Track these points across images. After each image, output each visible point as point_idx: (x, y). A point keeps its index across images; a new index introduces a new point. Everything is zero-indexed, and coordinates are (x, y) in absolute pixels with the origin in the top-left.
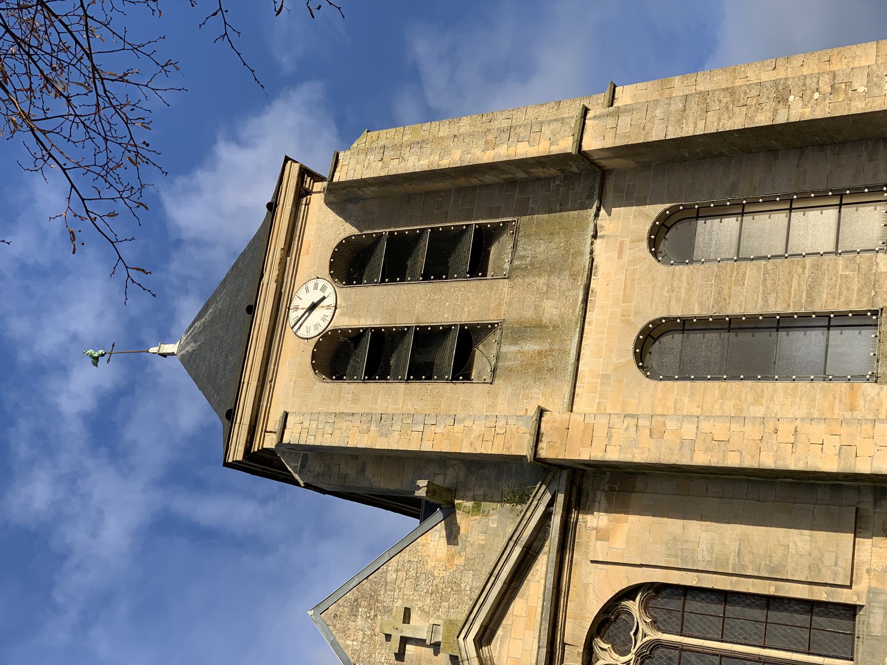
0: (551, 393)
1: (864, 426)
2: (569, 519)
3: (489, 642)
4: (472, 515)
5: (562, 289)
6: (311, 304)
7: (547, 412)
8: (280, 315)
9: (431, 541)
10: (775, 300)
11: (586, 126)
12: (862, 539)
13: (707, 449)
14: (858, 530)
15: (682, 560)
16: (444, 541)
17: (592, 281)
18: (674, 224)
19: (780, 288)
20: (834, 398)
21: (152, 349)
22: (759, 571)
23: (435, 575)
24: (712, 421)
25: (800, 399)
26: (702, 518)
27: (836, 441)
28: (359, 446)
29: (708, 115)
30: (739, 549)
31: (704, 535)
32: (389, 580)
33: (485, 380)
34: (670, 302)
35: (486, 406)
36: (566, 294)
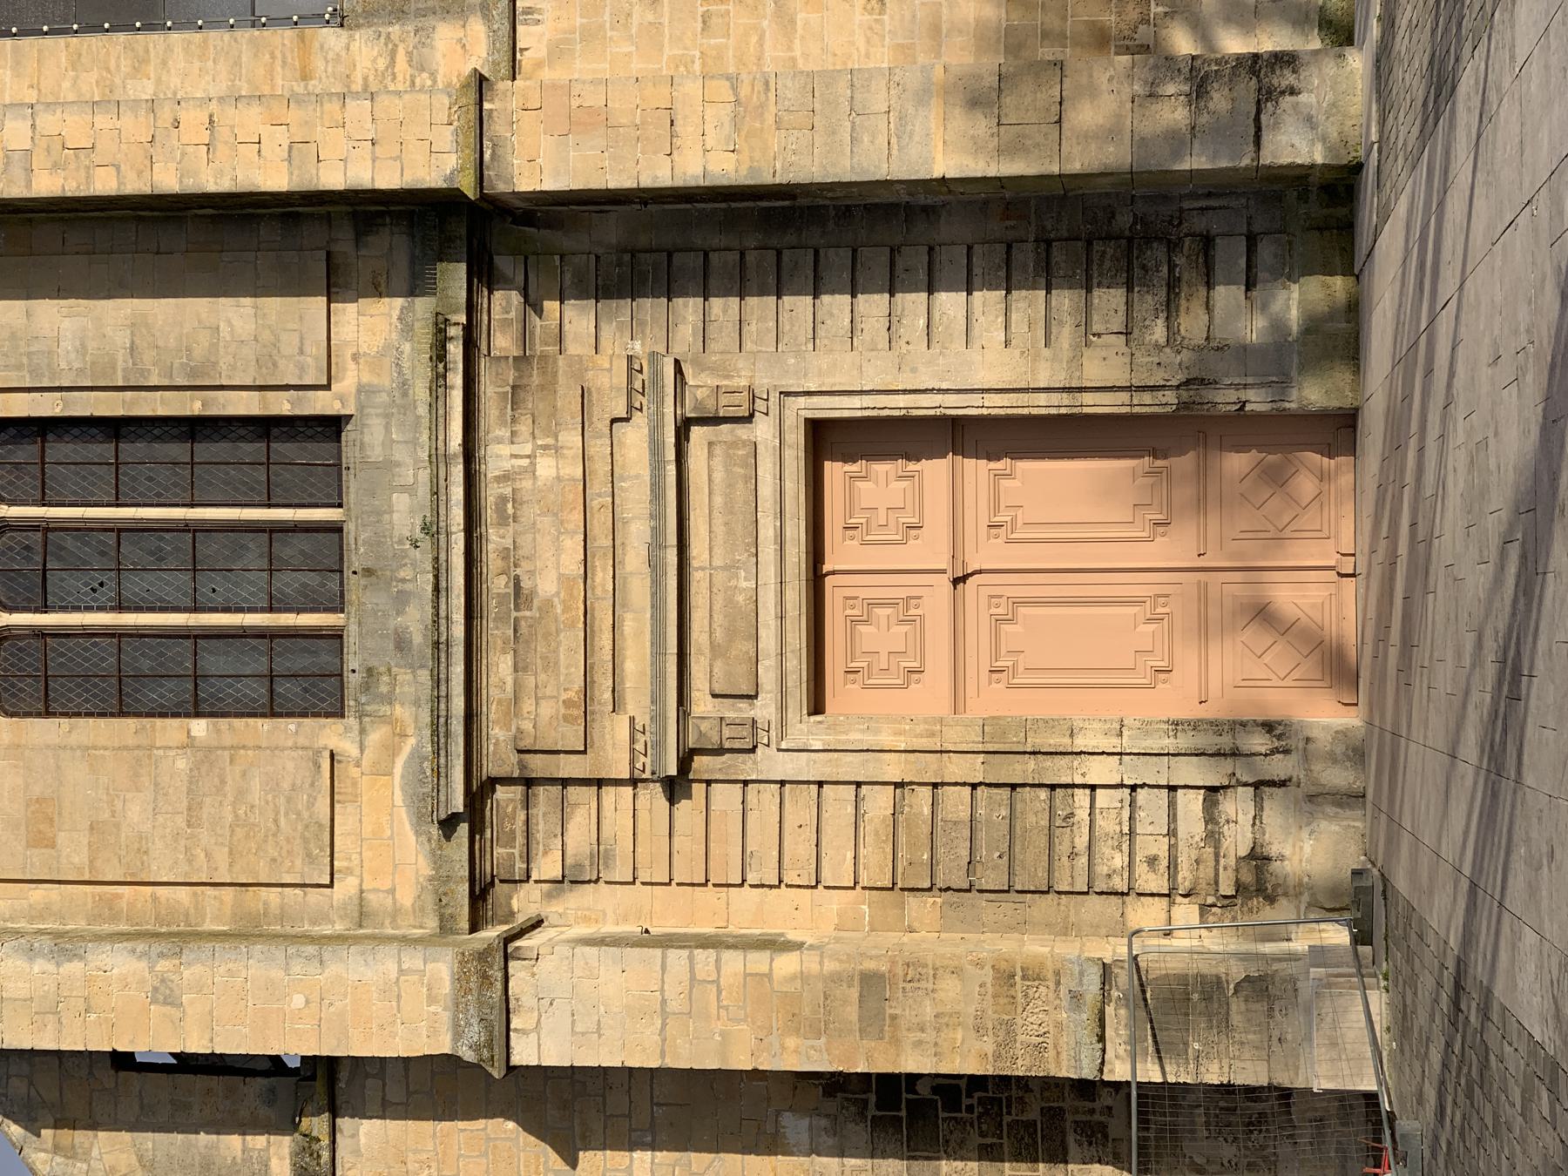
1: (327, 106)
13: (56, 166)
14: (333, 290)
20: (273, 57)
26: (60, 293)
30: (133, 342)
31: (66, 323)
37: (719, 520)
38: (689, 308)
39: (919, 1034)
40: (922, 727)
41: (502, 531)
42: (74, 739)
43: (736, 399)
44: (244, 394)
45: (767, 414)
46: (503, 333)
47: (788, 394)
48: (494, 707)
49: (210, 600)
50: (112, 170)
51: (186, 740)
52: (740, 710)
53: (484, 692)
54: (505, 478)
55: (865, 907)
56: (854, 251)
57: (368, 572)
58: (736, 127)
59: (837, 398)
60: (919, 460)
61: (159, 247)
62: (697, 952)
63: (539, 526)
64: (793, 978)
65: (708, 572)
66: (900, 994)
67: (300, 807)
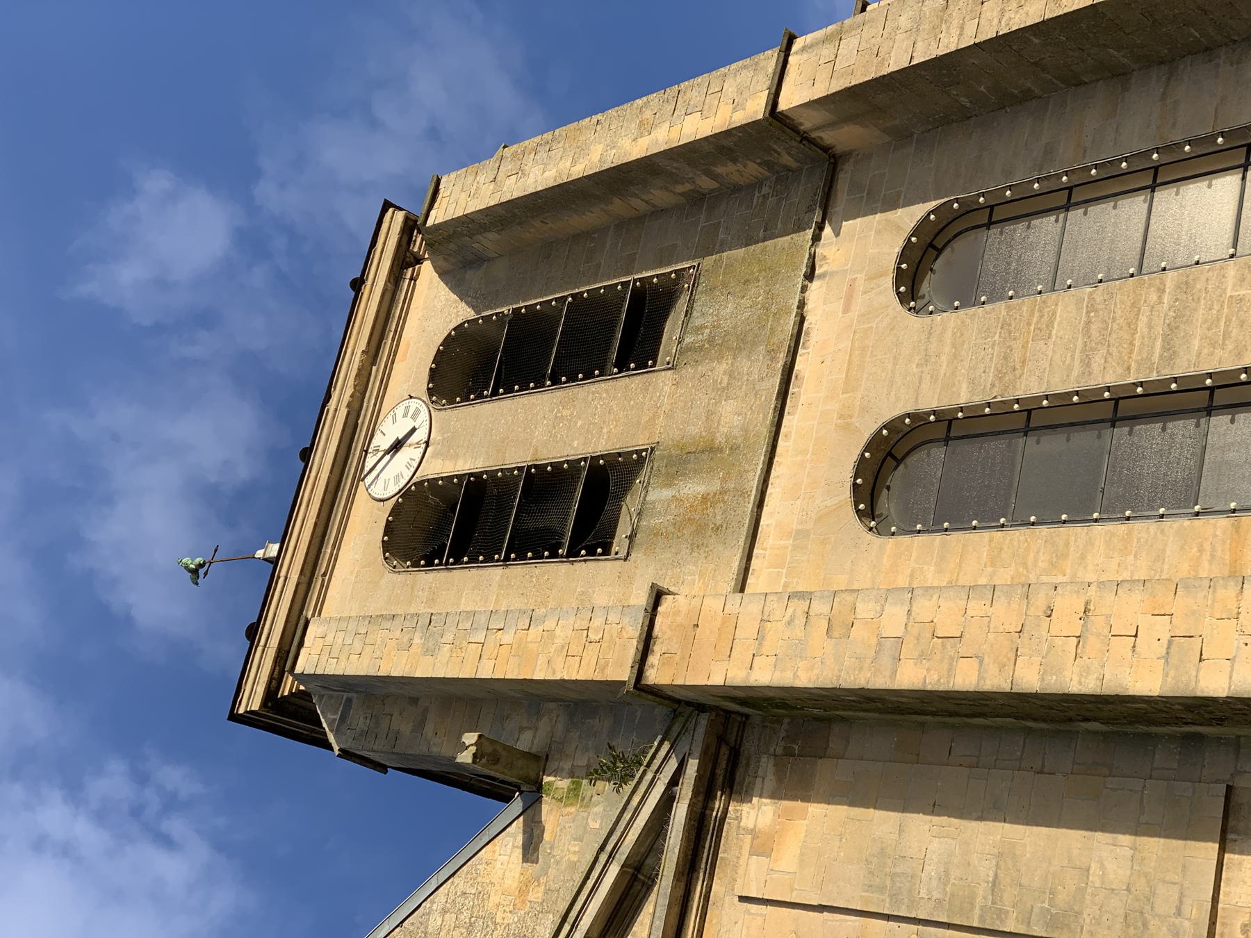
0: (713, 572)
1: (1221, 593)
2: (708, 812)
4: (565, 806)
5: (751, 379)
6: (395, 441)
7: (668, 596)
8: (352, 462)
9: (500, 855)
10: (1103, 361)
11: (788, 66)
12: (1236, 856)
14: (1231, 836)
15: (891, 896)
16: (518, 853)
18: (949, 241)
19: (1114, 336)
20: (1201, 550)
21: (258, 552)
22: (1029, 923)
23: (497, 921)
24: (935, 597)
25: (1135, 556)
26: (934, 809)
27: (1162, 627)
28: (393, 674)
29: (985, 9)
30: (996, 875)
31: (935, 845)
33: (617, 553)
34: (920, 383)
35: (613, 600)
36: (757, 387)
50: (975, 662)
61: (1043, 765)
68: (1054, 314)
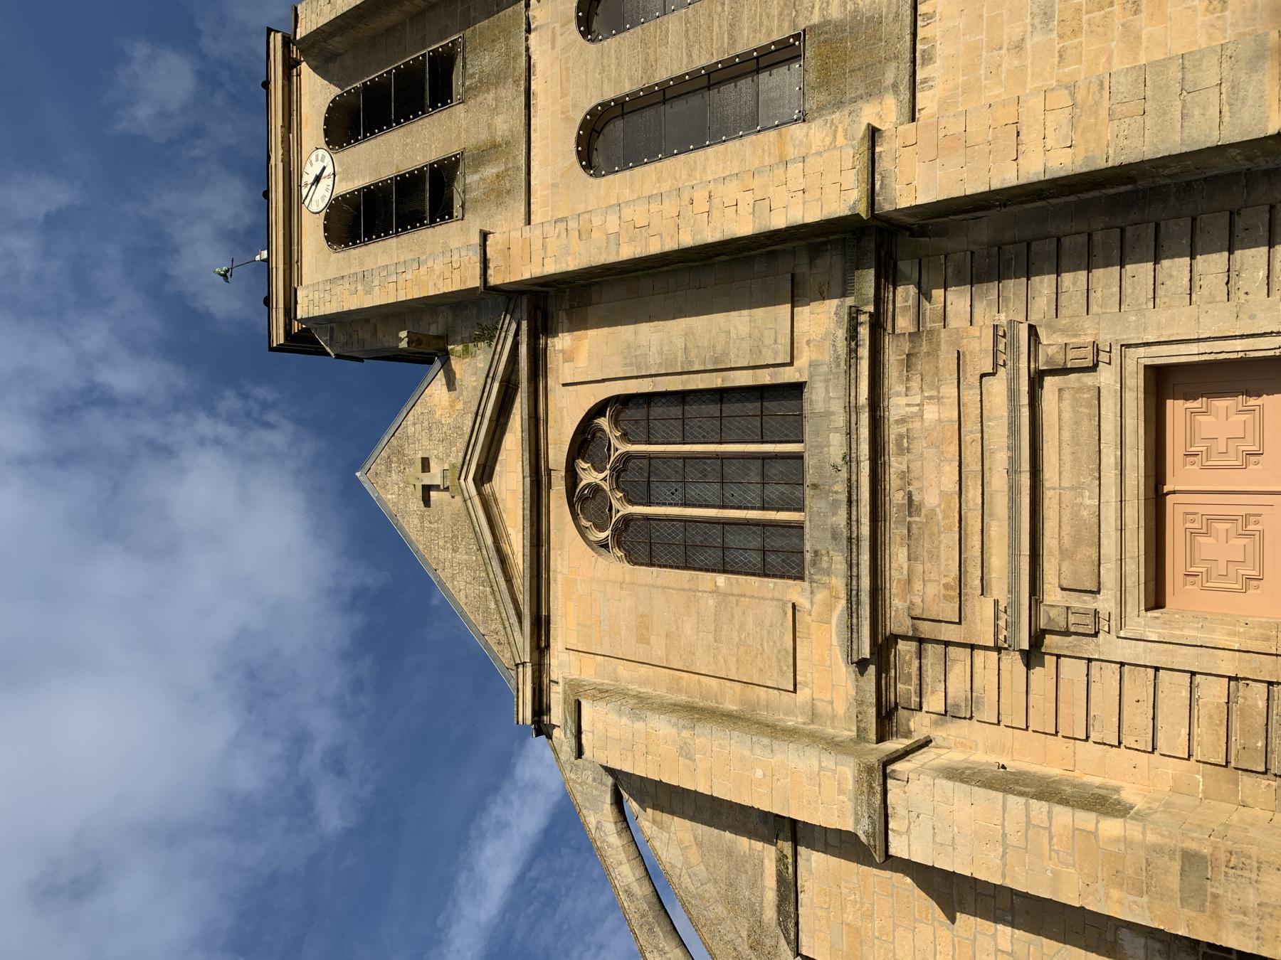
1: (776, 172)
3: (490, 479)
13: (631, 240)
16: (445, 388)
17: (532, 82)
20: (763, 151)
24: (632, 207)
26: (651, 319)
27: (749, 198)
28: (352, 308)
31: (654, 337)
32: (409, 434)
37: (1067, 450)
38: (1044, 284)
39: (1241, 916)
40: (1257, 631)
41: (900, 459)
42: (659, 582)
43: (1082, 353)
44: (745, 372)
45: (1110, 364)
46: (903, 316)
47: (1129, 346)
48: (895, 584)
49: (731, 501)
50: (658, 237)
51: (714, 588)
52: (1085, 602)
53: (888, 573)
54: (902, 421)
55: (1199, 777)
56: (1194, 219)
57: (815, 486)
58: (1073, 127)
59: (1175, 346)
60: (1259, 396)
62: (1033, 802)
63: (926, 456)
64: (1116, 841)
65: (1058, 491)
66: (1222, 877)
67: (775, 638)
68: (668, 28)
